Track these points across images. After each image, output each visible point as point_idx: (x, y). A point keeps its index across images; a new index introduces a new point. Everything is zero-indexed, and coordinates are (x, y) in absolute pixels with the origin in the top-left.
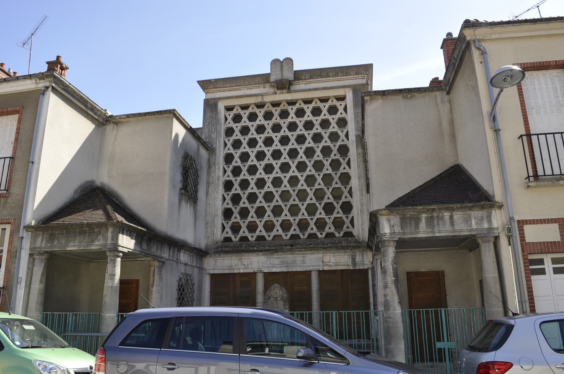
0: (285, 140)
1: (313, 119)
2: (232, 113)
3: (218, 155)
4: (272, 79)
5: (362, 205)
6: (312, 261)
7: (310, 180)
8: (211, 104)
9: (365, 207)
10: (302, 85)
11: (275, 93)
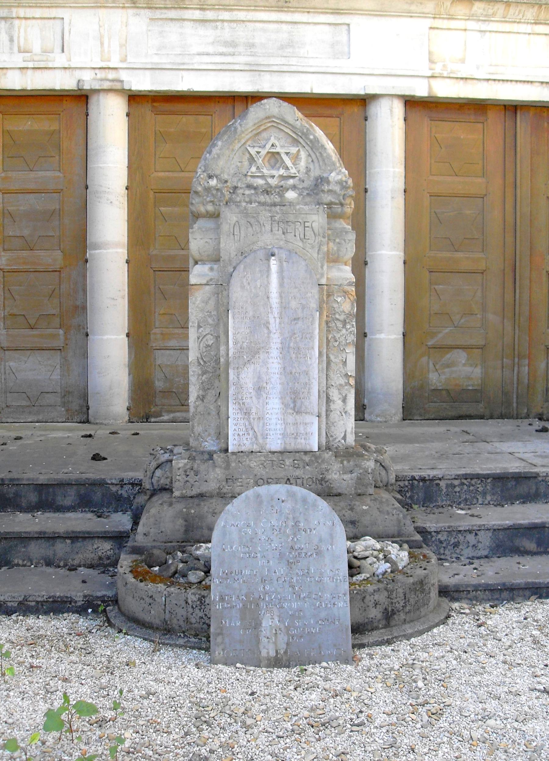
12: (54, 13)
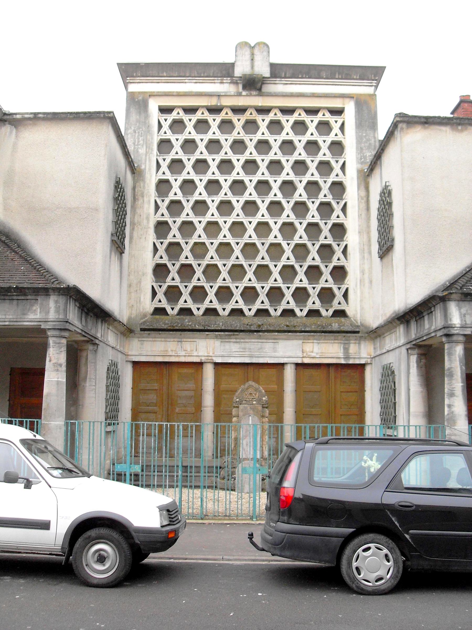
0: (251, 166)
1: (206, 156)
2: (171, 118)
3: (147, 181)
4: (238, 72)
5: (363, 272)
6: (288, 351)
7: (288, 229)
8: (139, 101)
9: (366, 276)
10: (280, 87)
11: (239, 95)
12: (194, 340)
